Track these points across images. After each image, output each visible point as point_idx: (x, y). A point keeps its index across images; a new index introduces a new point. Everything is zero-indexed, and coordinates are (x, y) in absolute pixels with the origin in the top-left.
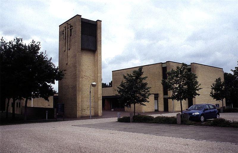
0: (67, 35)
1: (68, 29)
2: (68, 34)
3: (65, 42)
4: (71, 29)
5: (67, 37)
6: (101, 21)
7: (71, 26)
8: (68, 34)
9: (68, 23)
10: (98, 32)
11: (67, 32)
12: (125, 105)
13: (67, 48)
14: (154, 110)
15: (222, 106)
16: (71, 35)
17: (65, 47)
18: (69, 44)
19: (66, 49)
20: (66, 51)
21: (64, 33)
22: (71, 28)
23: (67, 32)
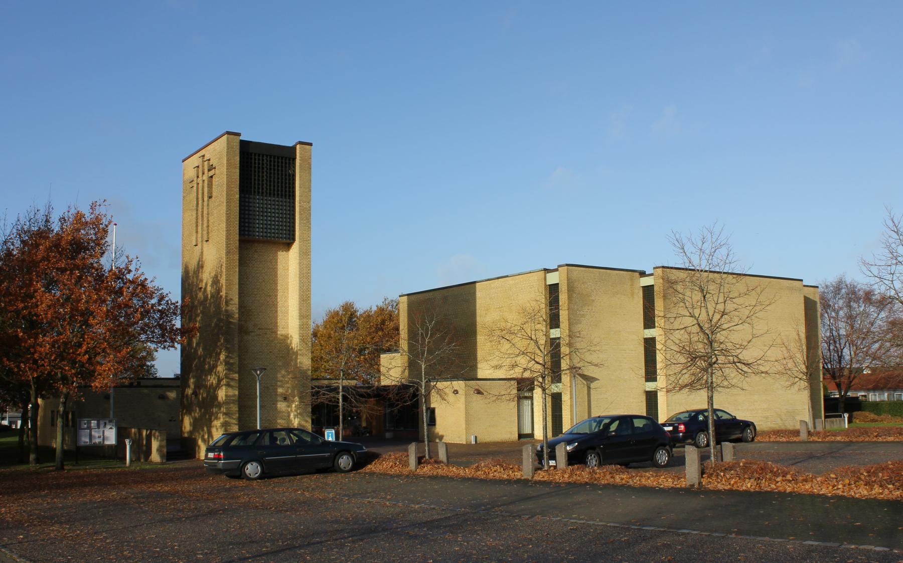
0: (200, 196)
1: (203, 174)
2: (203, 193)
3: (197, 218)
4: (212, 177)
5: (200, 202)
6: (311, 144)
7: (211, 168)
8: (203, 193)
9: (203, 156)
10: (275, 282)
11: (200, 185)
12: (684, 433)
13: (202, 237)
14: (432, 406)
15: (586, 417)
16: (210, 197)
17: (197, 232)
18: (205, 225)
19: (200, 240)
20: (199, 245)
21: (195, 188)
22: (211, 173)
23: (200, 185)
